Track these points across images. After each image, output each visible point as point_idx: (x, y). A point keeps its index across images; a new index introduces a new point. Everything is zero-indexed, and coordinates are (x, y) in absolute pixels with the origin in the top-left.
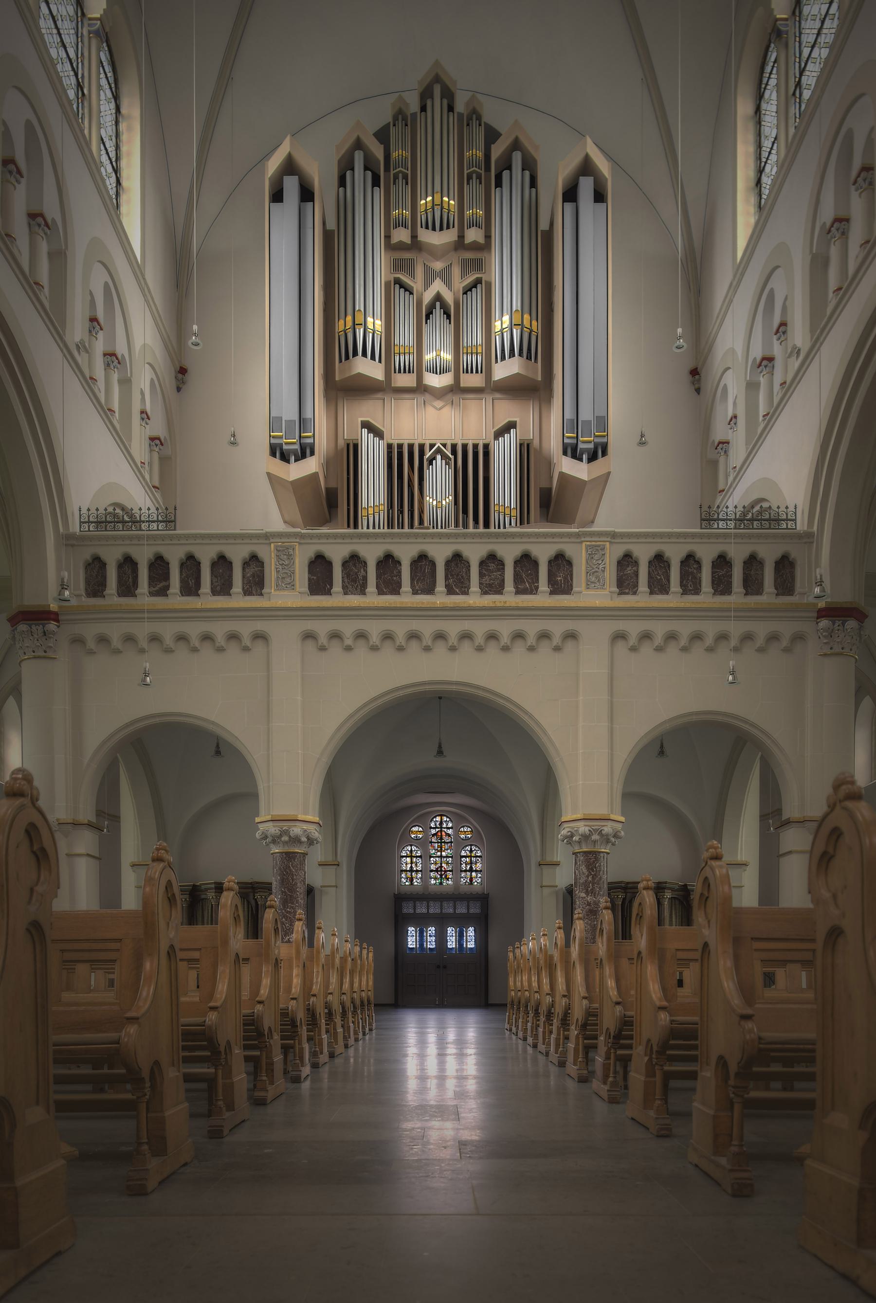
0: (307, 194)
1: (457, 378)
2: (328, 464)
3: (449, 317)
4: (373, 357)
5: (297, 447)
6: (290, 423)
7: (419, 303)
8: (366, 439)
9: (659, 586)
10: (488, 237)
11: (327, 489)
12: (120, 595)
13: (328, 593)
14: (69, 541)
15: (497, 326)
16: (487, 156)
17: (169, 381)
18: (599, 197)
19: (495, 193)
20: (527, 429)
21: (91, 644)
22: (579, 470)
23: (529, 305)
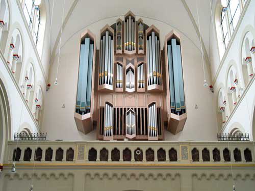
0: (92, 42)
1: (136, 89)
2: (94, 114)
3: (133, 73)
4: (110, 84)
5: (85, 110)
6: (83, 103)
7: (124, 69)
8: (107, 107)
9: (206, 159)
10: (145, 52)
11: (93, 121)
12: (24, 160)
13: (95, 160)
14: (10, 143)
15: (148, 76)
16: (144, 31)
17: (44, 90)
18: (178, 43)
19: (147, 42)
20: (159, 102)
21: (12, 177)
22: (176, 117)
23: (158, 70)
